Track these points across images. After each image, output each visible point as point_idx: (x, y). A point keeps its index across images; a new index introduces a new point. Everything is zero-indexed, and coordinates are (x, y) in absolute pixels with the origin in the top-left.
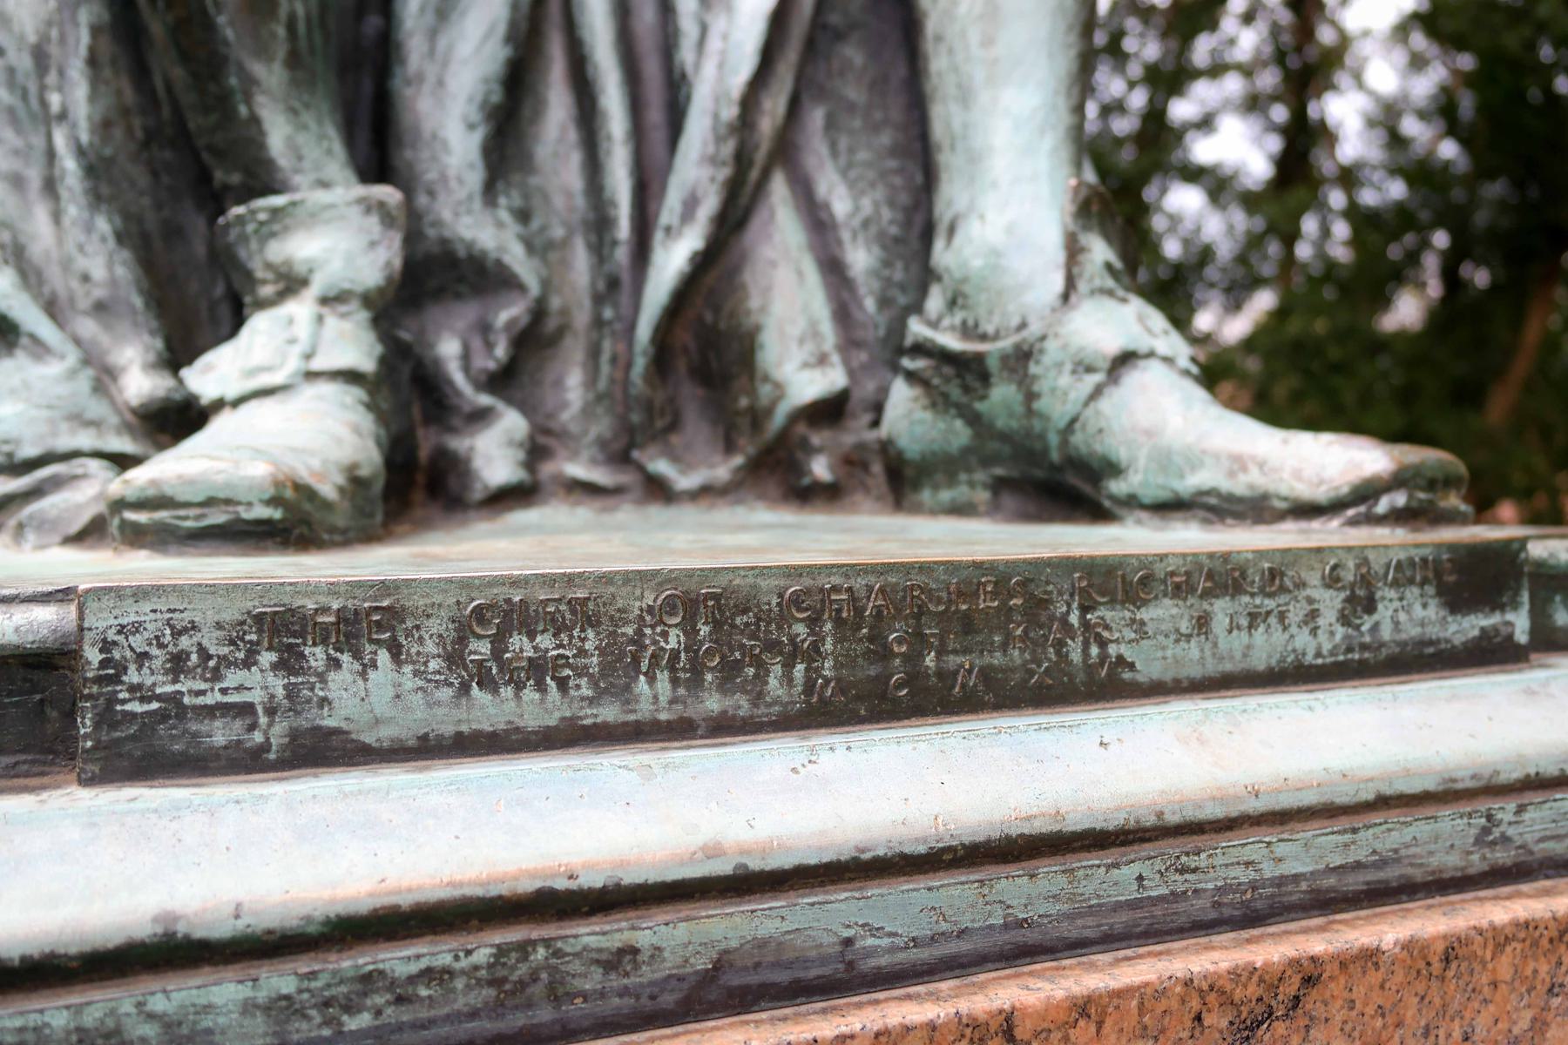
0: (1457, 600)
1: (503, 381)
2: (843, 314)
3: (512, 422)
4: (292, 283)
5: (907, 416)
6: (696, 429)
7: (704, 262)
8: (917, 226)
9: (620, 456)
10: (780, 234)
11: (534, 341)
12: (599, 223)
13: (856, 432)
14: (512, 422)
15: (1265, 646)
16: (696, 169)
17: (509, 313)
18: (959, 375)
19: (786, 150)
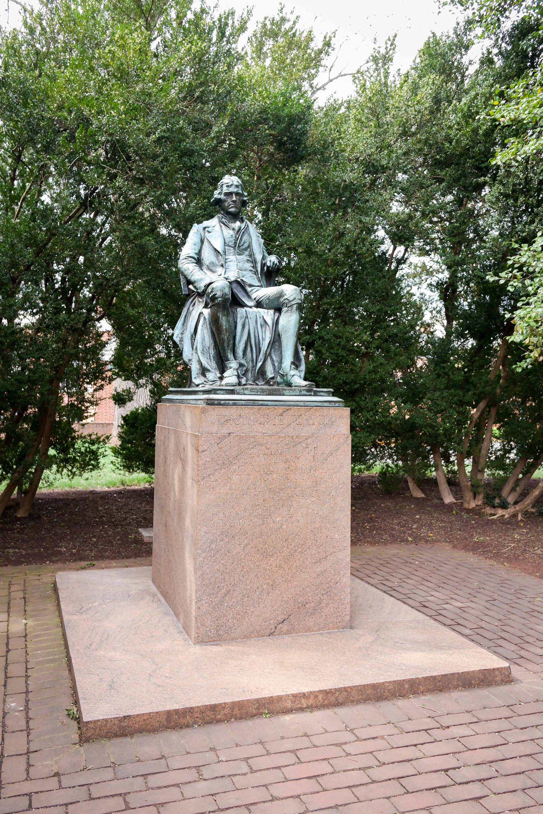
0: (307, 392)
1: (243, 375)
2: (274, 369)
3: (245, 378)
4: (231, 368)
5: (279, 379)
6: (261, 379)
7: (262, 365)
8: (281, 362)
9: (254, 382)
10: (269, 362)
11: (246, 371)
12: (253, 360)
13: (275, 380)
14: (245, 378)
15: (294, 394)
16: (261, 356)
17: (245, 368)
18: (282, 376)
19: (270, 354)
